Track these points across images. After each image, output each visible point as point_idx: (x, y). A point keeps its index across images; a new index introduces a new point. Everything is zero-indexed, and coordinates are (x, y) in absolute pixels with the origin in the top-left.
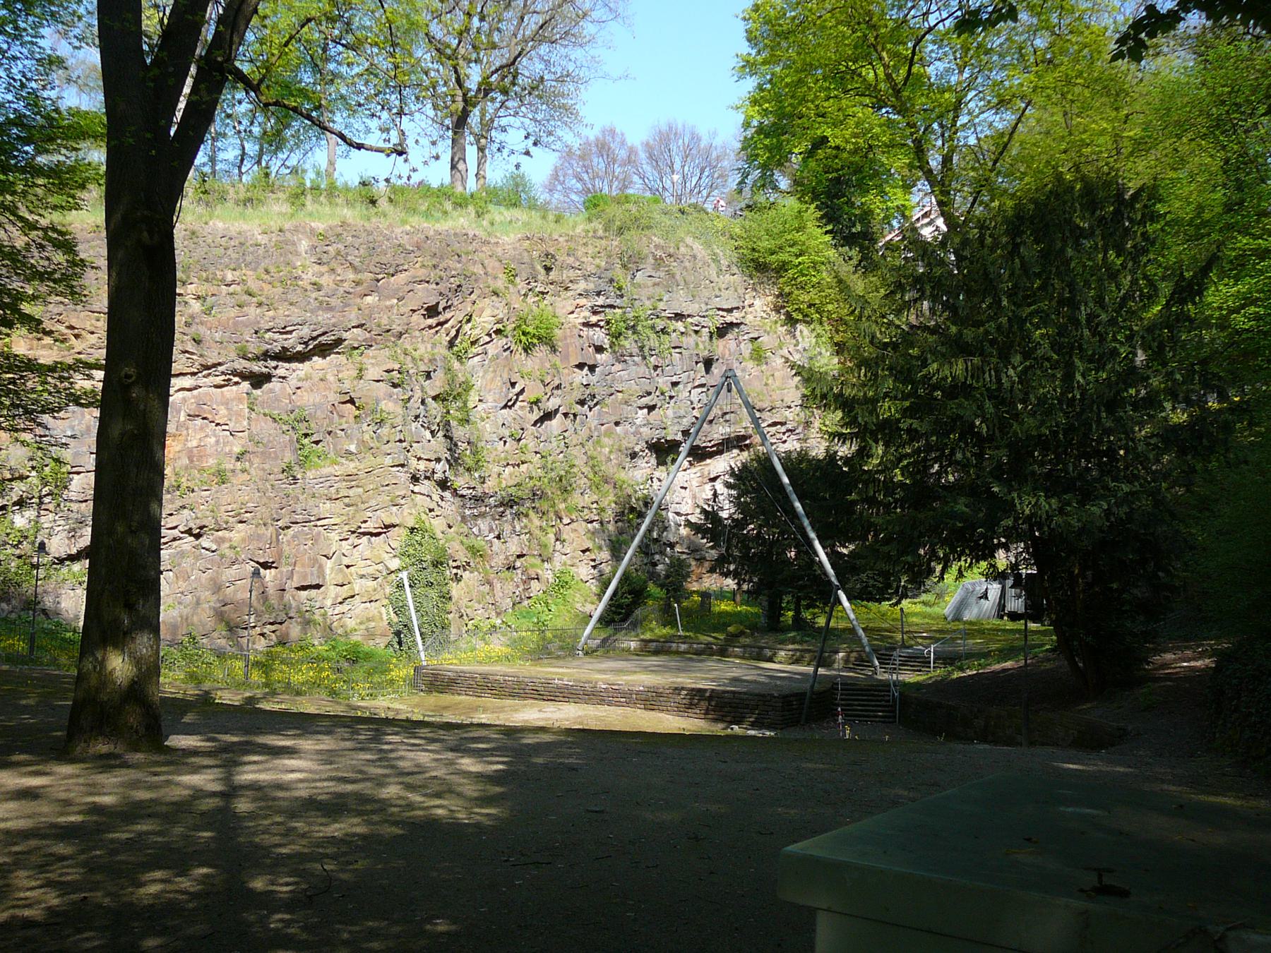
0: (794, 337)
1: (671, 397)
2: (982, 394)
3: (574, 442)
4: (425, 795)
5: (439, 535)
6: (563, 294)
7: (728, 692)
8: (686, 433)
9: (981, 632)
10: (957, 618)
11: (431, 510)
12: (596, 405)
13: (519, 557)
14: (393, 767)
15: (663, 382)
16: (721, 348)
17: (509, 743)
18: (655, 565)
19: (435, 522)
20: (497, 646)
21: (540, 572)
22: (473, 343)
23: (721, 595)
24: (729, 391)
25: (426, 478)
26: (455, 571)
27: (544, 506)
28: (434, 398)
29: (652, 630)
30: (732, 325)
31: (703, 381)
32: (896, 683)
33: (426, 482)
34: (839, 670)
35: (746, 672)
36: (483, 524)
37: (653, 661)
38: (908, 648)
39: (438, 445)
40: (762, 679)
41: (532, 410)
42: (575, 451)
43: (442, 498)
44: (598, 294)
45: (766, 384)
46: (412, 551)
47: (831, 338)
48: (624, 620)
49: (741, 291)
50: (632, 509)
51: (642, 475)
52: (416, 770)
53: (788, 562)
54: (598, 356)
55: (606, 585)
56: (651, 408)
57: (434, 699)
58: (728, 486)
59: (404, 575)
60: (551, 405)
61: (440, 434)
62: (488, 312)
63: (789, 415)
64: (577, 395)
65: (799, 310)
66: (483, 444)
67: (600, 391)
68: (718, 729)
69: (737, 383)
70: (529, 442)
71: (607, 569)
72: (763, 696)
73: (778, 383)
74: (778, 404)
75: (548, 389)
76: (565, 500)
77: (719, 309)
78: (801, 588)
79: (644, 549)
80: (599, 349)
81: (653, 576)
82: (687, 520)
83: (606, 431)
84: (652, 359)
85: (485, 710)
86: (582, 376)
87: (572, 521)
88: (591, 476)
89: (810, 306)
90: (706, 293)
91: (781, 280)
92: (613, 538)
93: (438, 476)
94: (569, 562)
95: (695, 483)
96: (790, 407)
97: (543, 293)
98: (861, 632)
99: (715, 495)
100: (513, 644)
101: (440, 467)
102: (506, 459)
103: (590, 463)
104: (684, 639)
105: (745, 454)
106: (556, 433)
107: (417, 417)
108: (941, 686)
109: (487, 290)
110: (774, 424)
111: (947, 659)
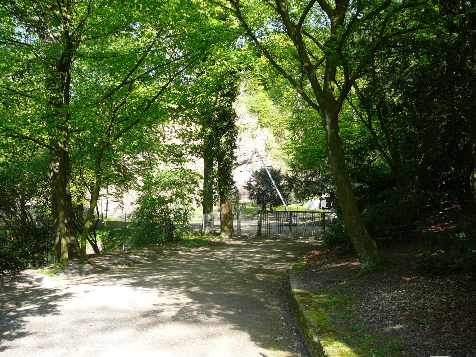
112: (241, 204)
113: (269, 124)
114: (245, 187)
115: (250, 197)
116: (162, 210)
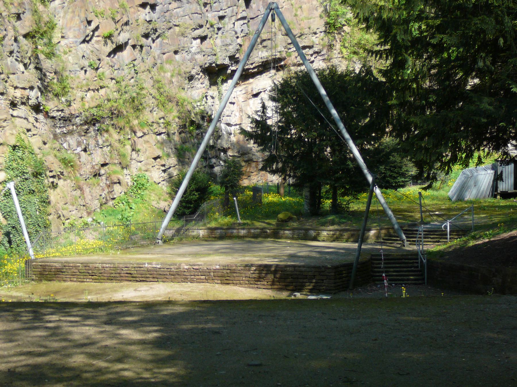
1: (219, 29)
2: (502, 11)
3: (143, 69)
4: (107, 361)
5: (37, 151)
9: (482, 209)
10: (460, 198)
11: (29, 130)
12: (158, 37)
13: (103, 165)
14: (65, 340)
15: (212, 16)
17: (150, 315)
18: (212, 167)
19: (33, 140)
20: (91, 239)
21: (121, 177)
23: (268, 189)
24: (273, 20)
25: (23, 103)
26: (51, 180)
27: (121, 122)
28: (25, 36)
29: (216, 220)
31: (244, 14)
32: (424, 253)
33: (22, 107)
34: (371, 244)
35: (299, 249)
36: (72, 140)
38: (427, 223)
39: (31, 76)
40: (314, 254)
41: (106, 43)
42: (143, 76)
43: (36, 120)
45: (296, 15)
46: (15, 165)
48: (193, 213)
50: (192, 123)
51: (199, 94)
52: (86, 341)
53: (325, 160)
55: (178, 185)
56: (203, 39)
58: (273, 99)
59: (11, 185)
60: (122, 38)
61: (32, 66)
63: (316, 40)
64: (142, 30)
66: (67, 73)
67: (161, 26)
68: (284, 295)
69: (280, 14)
70: (105, 70)
71: (175, 172)
72: (319, 267)
73: (305, 14)
74: (306, 31)
75: (119, 26)
76: (138, 117)
78: (337, 180)
79: (205, 157)
81: (213, 176)
82: (242, 129)
83: (168, 59)
85: (90, 293)
86: (145, 14)
87: (145, 134)
93: (32, 102)
94: (144, 168)
95: (241, 99)
96: (315, 33)
98: (390, 213)
99: (264, 107)
100: (104, 237)
101: (34, 94)
103: (157, 86)
104: (243, 226)
105: (281, 73)
106: (127, 62)
107: (11, 52)
108: (460, 253)
111: (460, 231)
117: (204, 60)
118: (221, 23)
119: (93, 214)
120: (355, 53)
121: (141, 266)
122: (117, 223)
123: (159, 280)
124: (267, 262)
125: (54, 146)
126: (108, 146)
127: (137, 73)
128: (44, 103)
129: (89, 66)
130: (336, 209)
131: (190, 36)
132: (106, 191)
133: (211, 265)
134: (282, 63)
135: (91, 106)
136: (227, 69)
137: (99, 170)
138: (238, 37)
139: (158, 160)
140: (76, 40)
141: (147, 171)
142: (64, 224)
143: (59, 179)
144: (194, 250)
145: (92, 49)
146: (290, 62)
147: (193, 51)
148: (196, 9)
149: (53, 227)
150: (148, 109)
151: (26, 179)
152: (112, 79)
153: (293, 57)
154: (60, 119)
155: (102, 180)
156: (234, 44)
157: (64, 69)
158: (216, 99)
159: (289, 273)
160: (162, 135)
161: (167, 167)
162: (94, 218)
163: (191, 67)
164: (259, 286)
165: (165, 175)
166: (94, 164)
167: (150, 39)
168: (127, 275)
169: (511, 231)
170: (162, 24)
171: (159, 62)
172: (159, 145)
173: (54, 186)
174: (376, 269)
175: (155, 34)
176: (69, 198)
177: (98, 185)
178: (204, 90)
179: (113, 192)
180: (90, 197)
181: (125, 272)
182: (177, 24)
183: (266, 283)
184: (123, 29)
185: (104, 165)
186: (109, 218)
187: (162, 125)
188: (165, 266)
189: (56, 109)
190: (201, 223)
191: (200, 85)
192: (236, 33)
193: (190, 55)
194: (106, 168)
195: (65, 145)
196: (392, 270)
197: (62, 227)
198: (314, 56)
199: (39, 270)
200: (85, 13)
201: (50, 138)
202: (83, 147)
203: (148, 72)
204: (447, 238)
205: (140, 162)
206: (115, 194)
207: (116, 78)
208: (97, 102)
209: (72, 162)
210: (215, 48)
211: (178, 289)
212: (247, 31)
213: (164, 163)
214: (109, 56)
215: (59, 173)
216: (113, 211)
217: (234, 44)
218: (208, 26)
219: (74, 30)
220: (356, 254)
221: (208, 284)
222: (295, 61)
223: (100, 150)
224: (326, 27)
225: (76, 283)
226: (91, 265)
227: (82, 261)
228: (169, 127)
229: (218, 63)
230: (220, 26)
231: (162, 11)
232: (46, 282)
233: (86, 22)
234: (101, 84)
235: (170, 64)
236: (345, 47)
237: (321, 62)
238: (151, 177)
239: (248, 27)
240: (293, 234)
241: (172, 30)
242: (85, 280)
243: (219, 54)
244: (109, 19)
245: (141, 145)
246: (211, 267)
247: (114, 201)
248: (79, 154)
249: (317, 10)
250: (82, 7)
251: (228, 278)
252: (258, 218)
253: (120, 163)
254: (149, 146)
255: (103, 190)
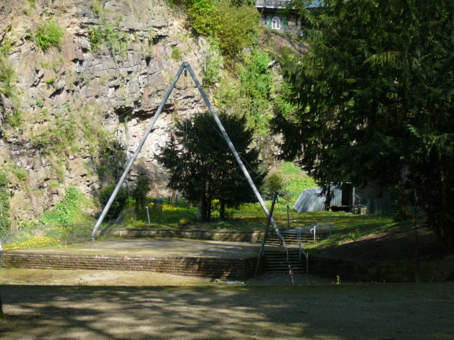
0: (198, 44)
1: (127, 81)
3: (74, 108)
6: (63, 15)
7: (210, 259)
8: (136, 103)
9: (320, 219)
10: (304, 210)
12: (84, 85)
15: (123, 71)
16: (155, 51)
20: (39, 236)
21: (59, 189)
22: (12, 45)
24: (186, 75)
26: (11, 190)
27: (59, 148)
30: (161, 37)
31: (146, 71)
36: (23, 160)
37: (140, 242)
41: (49, 87)
42: (74, 113)
44: (84, 15)
47: (220, 45)
49: (166, 16)
50: (108, 150)
51: (112, 128)
54: (84, 55)
56: (117, 87)
57: (14, 272)
60: (60, 84)
62: (21, 25)
64: (74, 78)
65: (200, 28)
67: (86, 76)
69: (190, 70)
70: (47, 108)
76: (70, 144)
77: (154, 27)
80: (85, 50)
84: (117, 57)
86: (75, 67)
87: (75, 157)
88: (84, 129)
89: (207, 25)
90: (147, 17)
91: (190, 10)
92: (99, 168)
94: (74, 183)
97: (52, 14)
102: (35, 119)
109: (20, 11)
110: (188, 97)
112: (150, 200)
113: (212, 29)
114: (160, 160)
115: (172, 185)
116: (89, 232)
117: (117, 103)
118: (129, 76)
119: (38, 217)
120: (224, 102)
121: (92, 257)
122: (58, 224)
123: (107, 268)
124: (191, 255)
125: (11, 164)
126: (49, 165)
127: (70, 111)
128: (5, 131)
129: (36, 104)
130: (223, 216)
131: (107, 85)
132: (47, 200)
133: (148, 257)
134: (171, 108)
135: (38, 135)
136: (132, 111)
137: (43, 183)
138: (140, 88)
139: (85, 177)
140: (28, 84)
141: (76, 185)
142: (18, 224)
143: (15, 189)
144: (124, 245)
145: (39, 92)
146: (177, 107)
147: (109, 97)
148: (113, 65)
149: (12, 227)
150: (78, 139)
151: (305, 182)
152: (53, 115)
153: (179, 104)
154: (15, 144)
155: (45, 191)
156: (138, 93)
157: (18, 106)
158: (124, 132)
159: (210, 264)
160: (87, 158)
161: (90, 182)
162: (40, 220)
163: (108, 108)
164: (186, 274)
165: (89, 189)
166: (39, 179)
167: (79, 86)
168: (80, 264)
169: (368, 234)
170: (87, 75)
171: (84, 103)
172: (85, 166)
173: (12, 195)
174: (268, 262)
175: (82, 82)
176: (22, 205)
177: (43, 195)
178: (116, 126)
179: (53, 201)
180: (36, 204)
181: (79, 262)
182: (98, 75)
183: (192, 272)
184: (61, 78)
185: (47, 180)
186: (51, 220)
187: (87, 151)
188: (111, 258)
189: (12, 136)
190: (122, 225)
191: (113, 122)
192: (140, 84)
193: (107, 99)
194: (47, 182)
195: (18, 164)
196: (281, 262)
197: (17, 226)
198: (194, 104)
199: (9, 259)
200: (35, 65)
201: (8, 158)
202: (32, 165)
203: (77, 111)
204: (313, 240)
205: (71, 178)
206: (54, 202)
207: (55, 114)
208: (43, 132)
209: (25, 176)
210: (124, 95)
211: (124, 275)
212: (147, 83)
213: (88, 179)
214: (50, 97)
215: (15, 185)
216: (53, 215)
217: (138, 93)
218: (120, 78)
219: (26, 77)
220: (261, 250)
221: (146, 272)
222: (181, 107)
223: (44, 168)
224: (203, 83)
225: (39, 270)
226: (51, 256)
227: (44, 253)
228: (92, 152)
229: (126, 106)
230: (129, 79)
231: (87, 66)
232: (14, 268)
233: (35, 71)
234: (45, 118)
235: (92, 105)
236: (217, 98)
237: (199, 108)
238: (80, 190)
239: (148, 80)
240: (192, 235)
241: (94, 80)
242: (46, 268)
243: (127, 99)
244: (51, 69)
245: (73, 165)
246: (149, 259)
247: (53, 208)
248: (28, 171)
249: (197, 70)
250: (32, 60)
251: (162, 267)
252: (163, 222)
253: (58, 179)
254: (78, 166)
255: (46, 199)
